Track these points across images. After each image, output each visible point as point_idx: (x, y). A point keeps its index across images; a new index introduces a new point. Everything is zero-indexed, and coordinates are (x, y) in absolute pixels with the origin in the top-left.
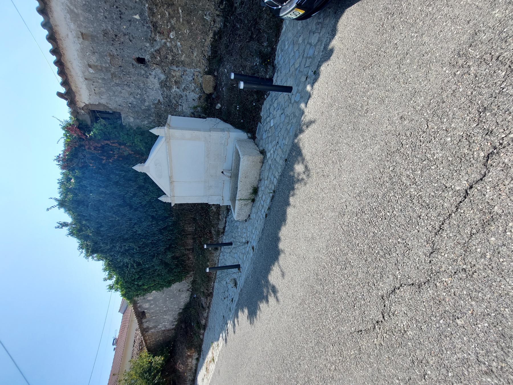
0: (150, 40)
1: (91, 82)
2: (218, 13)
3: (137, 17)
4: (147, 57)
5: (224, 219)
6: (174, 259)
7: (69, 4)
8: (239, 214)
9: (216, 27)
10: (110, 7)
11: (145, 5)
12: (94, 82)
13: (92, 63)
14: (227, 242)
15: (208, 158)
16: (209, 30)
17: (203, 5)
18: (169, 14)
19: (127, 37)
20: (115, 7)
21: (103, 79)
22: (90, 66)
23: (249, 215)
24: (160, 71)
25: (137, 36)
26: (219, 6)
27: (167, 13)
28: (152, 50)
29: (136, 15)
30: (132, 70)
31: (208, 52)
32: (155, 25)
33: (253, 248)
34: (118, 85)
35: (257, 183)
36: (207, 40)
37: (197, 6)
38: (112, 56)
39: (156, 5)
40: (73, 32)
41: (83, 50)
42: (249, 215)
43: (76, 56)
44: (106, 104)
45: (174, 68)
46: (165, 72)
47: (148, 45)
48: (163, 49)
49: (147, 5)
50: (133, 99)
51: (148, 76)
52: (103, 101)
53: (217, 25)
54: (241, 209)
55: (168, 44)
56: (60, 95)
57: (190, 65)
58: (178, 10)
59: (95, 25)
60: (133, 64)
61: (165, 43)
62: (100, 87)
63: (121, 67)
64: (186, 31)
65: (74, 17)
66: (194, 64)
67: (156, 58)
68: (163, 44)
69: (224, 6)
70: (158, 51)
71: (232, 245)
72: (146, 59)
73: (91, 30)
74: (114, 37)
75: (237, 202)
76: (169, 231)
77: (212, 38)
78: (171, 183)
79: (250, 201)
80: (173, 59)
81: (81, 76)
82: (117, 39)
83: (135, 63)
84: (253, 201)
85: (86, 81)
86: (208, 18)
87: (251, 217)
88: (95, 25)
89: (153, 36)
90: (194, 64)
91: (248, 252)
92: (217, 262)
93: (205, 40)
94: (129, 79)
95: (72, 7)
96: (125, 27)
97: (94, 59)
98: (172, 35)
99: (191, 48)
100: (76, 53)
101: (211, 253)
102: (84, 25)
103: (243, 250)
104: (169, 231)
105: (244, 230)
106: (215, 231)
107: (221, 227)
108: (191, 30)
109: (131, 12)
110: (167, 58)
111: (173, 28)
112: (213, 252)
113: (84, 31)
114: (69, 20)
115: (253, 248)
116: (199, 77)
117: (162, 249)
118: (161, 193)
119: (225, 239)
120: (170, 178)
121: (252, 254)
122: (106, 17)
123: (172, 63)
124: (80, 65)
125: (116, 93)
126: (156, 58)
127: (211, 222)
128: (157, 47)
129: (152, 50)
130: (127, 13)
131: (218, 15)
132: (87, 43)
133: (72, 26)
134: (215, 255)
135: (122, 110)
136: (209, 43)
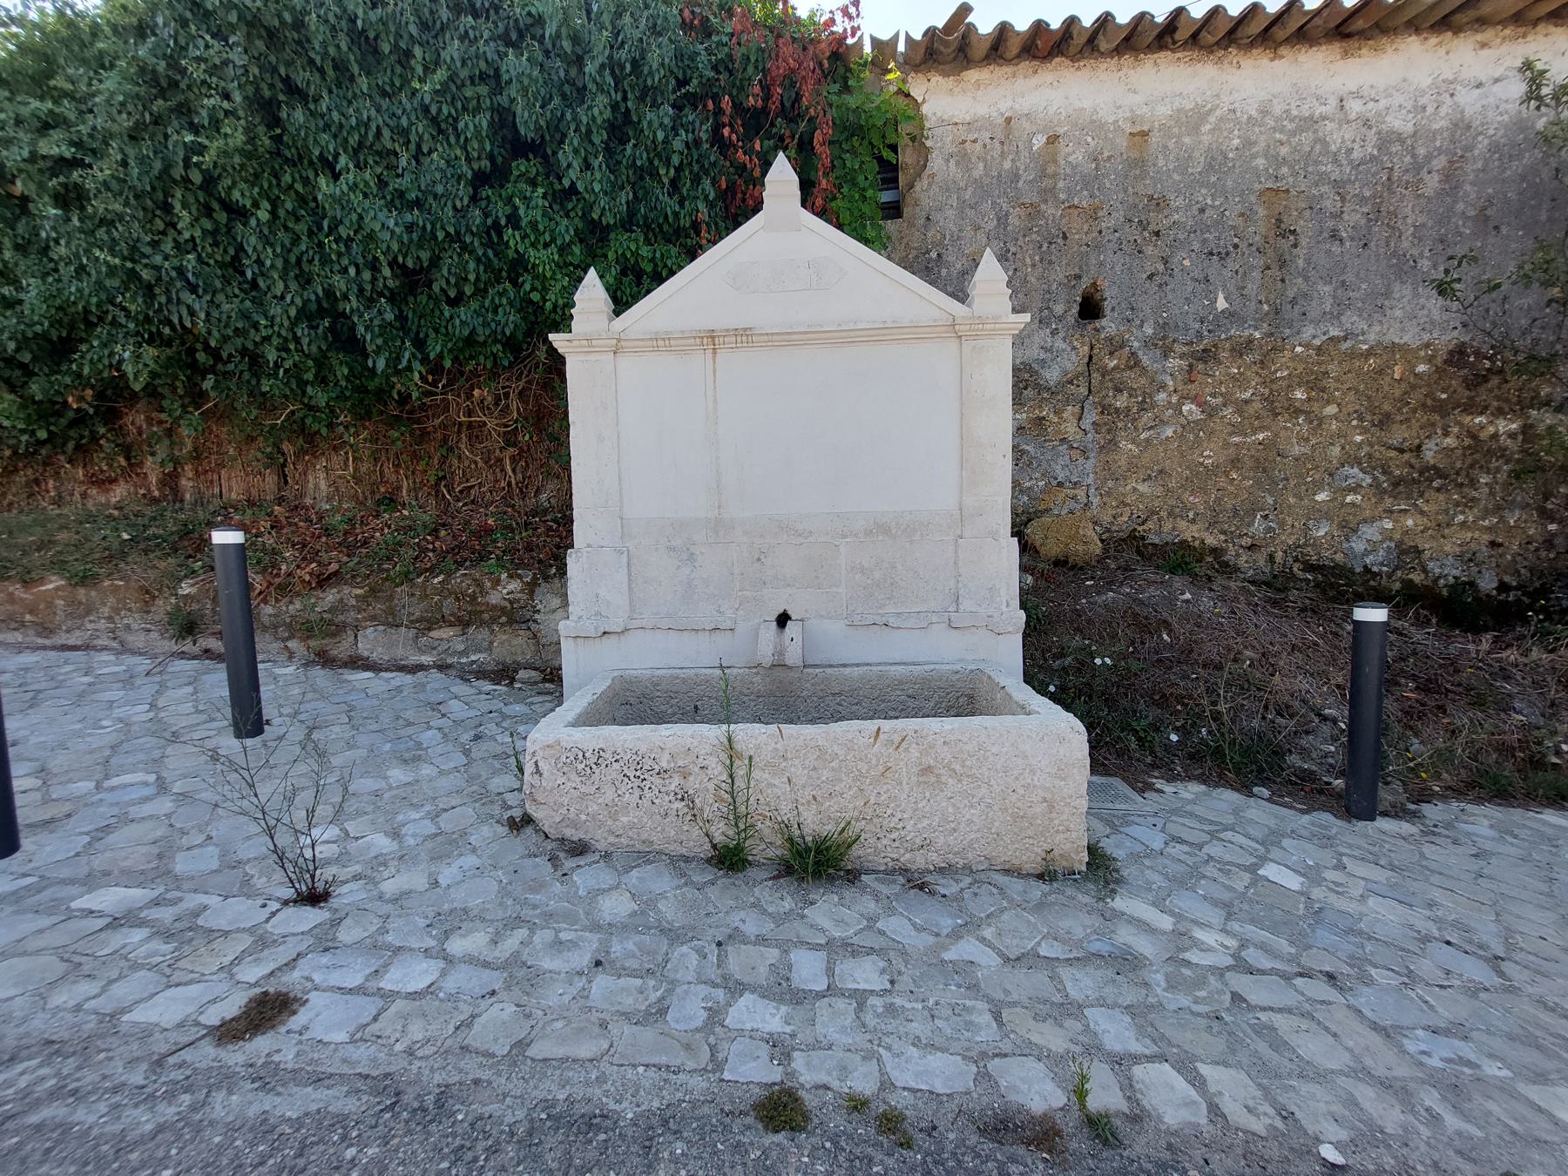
0: (1164, 338)
1: (1000, 135)
2: (1279, 556)
3: (1221, 304)
4: (1109, 325)
5: (426, 659)
6: (100, 396)
7: (1218, 113)
8: (590, 763)
9: (1238, 555)
10: (1234, 227)
11: (1256, 329)
12: (1002, 143)
13: (1064, 148)
14: (266, 691)
15: (869, 533)
16: (1224, 532)
17: (1289, 507)
18: (1246, 402)
19: (1161, 267)
20: (1236, 240)
21: (1016, 177)
22: (1053, 140)
23: (579, 849)
24: (1069, 366)
25: (1170, 297)
26: (1296, 560)
27: (1247, 395)
28: (1136, 344)
29: (1226, 299)
30: (1059, 273)
31: (1159, 533)
32: (1207, 356)
33: (269, 1010)
34: (1002, 220)
35: (881, 863)
36: (1194, 528)
37: (1285, 488)
38: (1093, 215)
39: (1262, 362)
40: (1145, 109)
41: (1096, 126)
42: (579, 849)
43: (1078, 104)
44: (928, 171)
45: (1091, 417)
46: (1071, 382)
47: (1149, 330)
48: (1143, 381)
49: (1257, 335)
50: (959, 266)
51: (1048, 324)
52: (936, 163)
53: (1244, 558)
54: (641, 770)
55: (1162, 396)
56: (965, 10)
57: (1107, 470)
58: (1262, 428)
59: (1176, 177)
60: (1078, 277)
61: (1163, 387)
62: (985, 160)
63: (1065, 237)
64: (1209, 456)
65: (1194, 119)
66: (1110, 484)
67: (1111, 353)
68: (1160, 378)
69: (1300, 574)
70: (1134, 363)
71: (240, 734)
72: (1104, 322)
73: (1161, 163)
74: (1152, 227)
75: (711, 733)
76: (321, 363)
77: (1203, 541)
78: (711, 339)
79: (721, 832)
80: (1117, 410)
81: (1017, 107)
82: (1146, 234)
83: (1085, 283)
84: (730, 860)
85: (1001, 121)
86: (1258, 526)
87: (587, 877)
88: (1176, 177)
89: (1177, 347)
90: (1110, 484)
91: (188, 933)
92: (61, 638)
93: (1193, 521)
94: (1028, 260)
95: (1212, 119)
96: (1187, 263)
97: (1074, 155)
98: (1190, 411)
99: (1161, 472)
100: (1087, 104)
101: (148, 596)
102: (1171, 145)
103: (209, 859)
104: (321, 363)
105: (417, 825)
106: (339, 607)
107: (370, 642)
108: (1213, 471)
109: (1231, 287)
110: (1118, 390)
111: (1211, 412)
112: (162, 607)
113: (1154, 139)
114: (1177, 105)
115: (269, 1010)
116: (1071, 504)
117: (193, 311)
118: (628, 289)
119: (281, 679)
120: (743, 336)
121: (165, 1010)
122: (1202, 211)
123: (1105, 409)
124: (1052, 110)
125: (970, 213)
126: (1111, 353)
127: (406, 577)
128: (1145, 360)
129: (1136, 344)
130: (1227, 273)
131: (1271, 557)
132: (1122, 142)
133: (1164, 110)
134: (135, 621)
135: (911, 225)
136: (1188, 536)
